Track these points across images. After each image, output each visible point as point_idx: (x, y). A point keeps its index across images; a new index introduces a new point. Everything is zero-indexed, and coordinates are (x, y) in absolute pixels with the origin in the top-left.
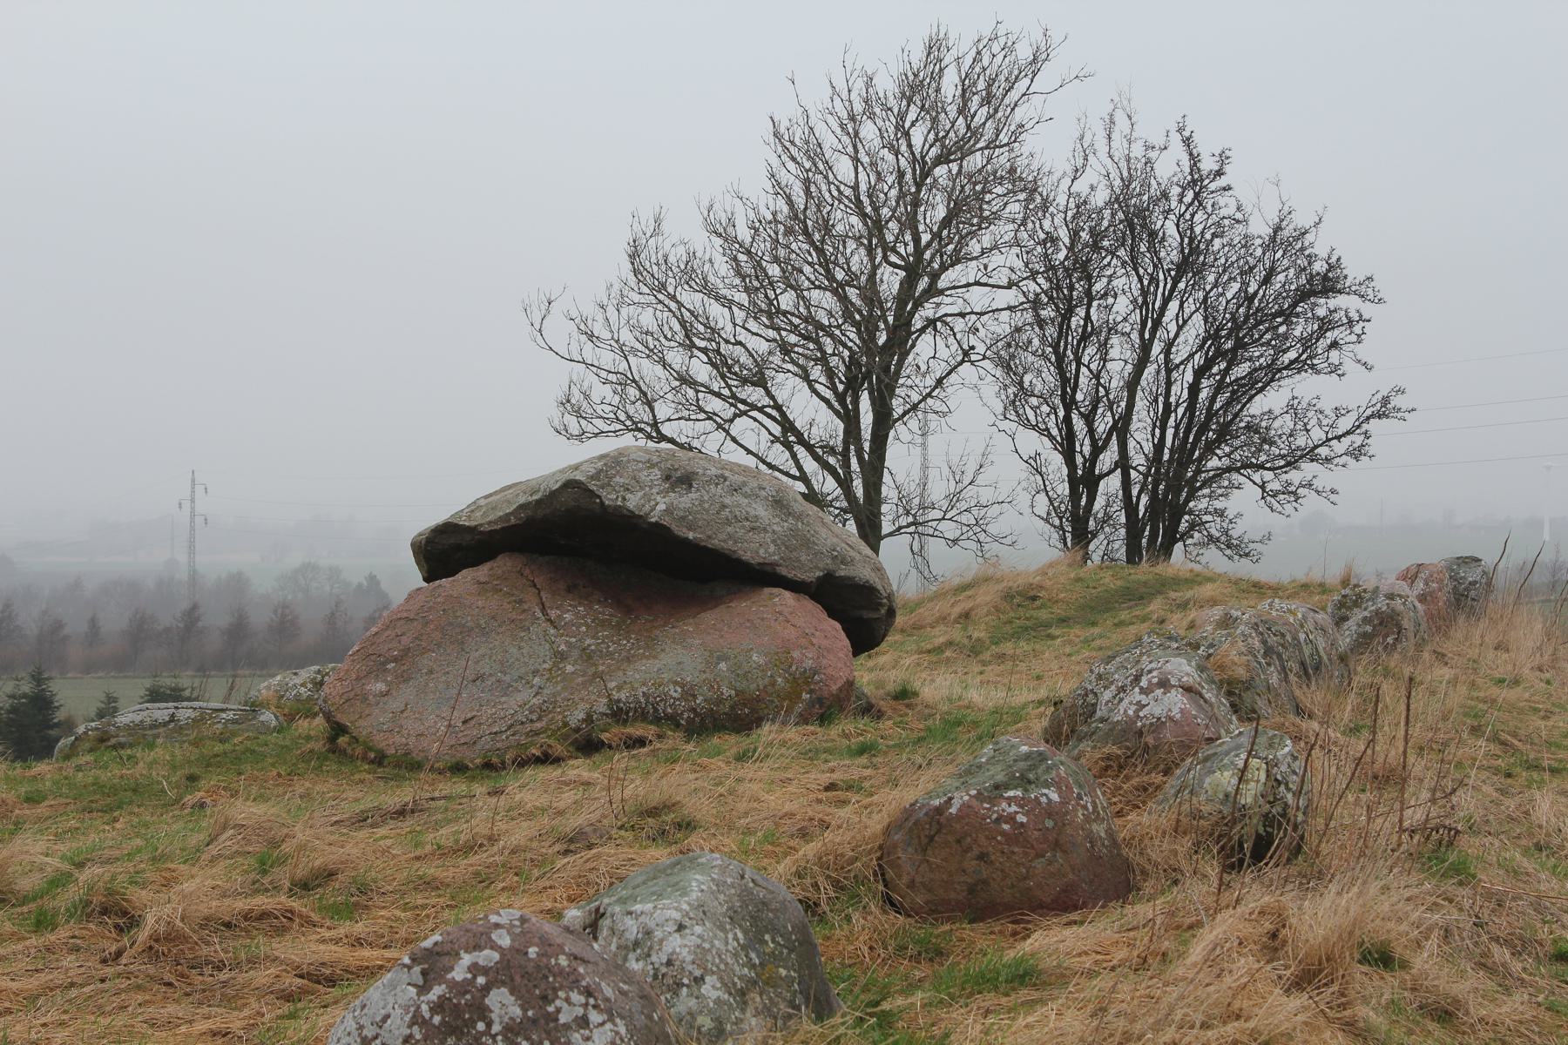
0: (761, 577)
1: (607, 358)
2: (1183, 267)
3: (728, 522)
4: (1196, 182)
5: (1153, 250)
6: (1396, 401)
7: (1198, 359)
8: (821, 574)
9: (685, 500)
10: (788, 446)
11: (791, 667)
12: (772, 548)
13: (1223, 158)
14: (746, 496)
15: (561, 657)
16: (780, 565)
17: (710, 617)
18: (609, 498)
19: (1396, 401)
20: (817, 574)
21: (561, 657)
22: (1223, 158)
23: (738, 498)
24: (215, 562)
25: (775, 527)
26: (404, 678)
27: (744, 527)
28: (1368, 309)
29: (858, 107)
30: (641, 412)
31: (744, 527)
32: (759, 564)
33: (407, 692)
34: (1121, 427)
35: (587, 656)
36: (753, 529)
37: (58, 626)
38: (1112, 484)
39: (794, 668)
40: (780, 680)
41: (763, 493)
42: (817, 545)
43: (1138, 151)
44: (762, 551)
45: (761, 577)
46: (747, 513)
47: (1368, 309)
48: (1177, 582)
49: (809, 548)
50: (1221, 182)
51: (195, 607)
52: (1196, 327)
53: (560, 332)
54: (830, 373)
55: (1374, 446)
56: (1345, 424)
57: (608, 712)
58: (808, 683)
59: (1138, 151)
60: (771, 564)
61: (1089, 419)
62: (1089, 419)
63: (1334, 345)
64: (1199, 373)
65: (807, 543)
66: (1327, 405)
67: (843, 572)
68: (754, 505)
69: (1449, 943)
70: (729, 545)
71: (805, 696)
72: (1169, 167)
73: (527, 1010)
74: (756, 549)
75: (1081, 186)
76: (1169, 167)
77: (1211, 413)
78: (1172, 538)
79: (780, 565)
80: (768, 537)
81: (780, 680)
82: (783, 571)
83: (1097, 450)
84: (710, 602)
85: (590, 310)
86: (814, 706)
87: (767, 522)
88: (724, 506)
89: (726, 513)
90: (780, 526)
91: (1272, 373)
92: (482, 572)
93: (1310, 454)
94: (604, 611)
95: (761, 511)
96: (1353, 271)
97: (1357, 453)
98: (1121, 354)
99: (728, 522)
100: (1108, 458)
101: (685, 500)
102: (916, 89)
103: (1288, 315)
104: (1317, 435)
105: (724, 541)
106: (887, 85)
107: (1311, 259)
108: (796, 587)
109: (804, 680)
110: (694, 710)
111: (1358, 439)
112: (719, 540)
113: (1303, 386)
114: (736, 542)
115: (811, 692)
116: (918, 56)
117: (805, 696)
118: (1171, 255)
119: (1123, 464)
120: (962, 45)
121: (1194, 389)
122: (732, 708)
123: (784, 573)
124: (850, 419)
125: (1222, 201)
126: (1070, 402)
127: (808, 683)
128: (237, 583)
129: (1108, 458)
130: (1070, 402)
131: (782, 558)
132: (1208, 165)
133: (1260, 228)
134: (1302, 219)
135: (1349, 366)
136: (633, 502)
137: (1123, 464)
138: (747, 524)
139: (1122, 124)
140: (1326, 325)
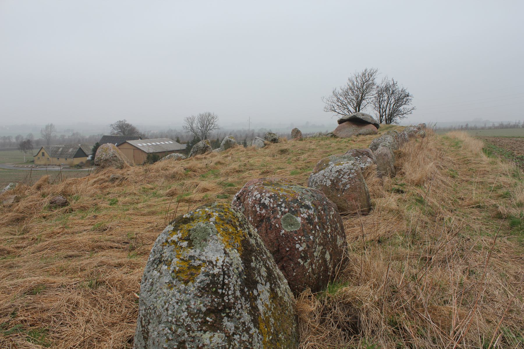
0: (369, 123)
1: (329, 103)
2: (392, 93)
4: (394, 84)
5: (389, 92)
6: (415, 108)
7: (394, 103)
9: (364, 117)
10: (348, 112)
13: (397, 82)
15: (354, 130)
17: (366, 127)
18: (357, 117)
19: (415, 108)
21: (354, 130)
22: (397, 82)
24: (252, 128)
26: (340, 131)
28: (412, 98)
29: (357, 76)
30: (333, 109)
33: (341, 132)
34: (385, 111)
35: (356, 129)
37: (237, 136)
38: (384, 117)
43: (388, 81)
45: (369, 123)
47: (412, 98)
48: (393, 126)
50: (396, 85)
51: (253, 133)
52: (393, 100)
53: (325, 100)
54: (353, 104)
55: (412, 113)
56: (409, 110)
59: (388, 81)
61: (382, 109)
62: (382, 109)
63: (408, 102)
64: (394, 105)
66: (407, 108)
69: (323, 332)
72: (391, 83)
74: (369, 121)
75: (382, 85)
76: (391, 83)
77: (395, 109)
78: (391, 122)
83: (383, 113)
84: (365, 125)
85: (328, 98)
90: (371, 119)
91: (401, 105)
92: (346, 123)
93: (405, 113)
94: (356, 126)
95: (369, 118)
96: (410, 94)
97: (411, 113)
98: (386, 103)
100: (384, 114)
101: (364, 117)
102: (364, 74)
103: (403, 99)
104: (406, 111)
106: (360, 74)
107: (406, 93)
108: (372, 124)
109: (374, 131)
111: (410, 112)
112: (366, 120)
113: (405, 106)
116: (364, 71)
118: (391, 92)
119: (385, 115)
120: (368, 71)
121: (393, 106)
124: (356, 110)
125: (396, 86)
126: (380, 108)
128: (253, 130)
129: (384, 114)
130: (380, 108)
132: (395, 83)
133: (400, 89)
134: (405, 89)
135: (410, 104)
136: (359, 117)
137: (385, 115)
139: (386, 78)
140: (407, 100)
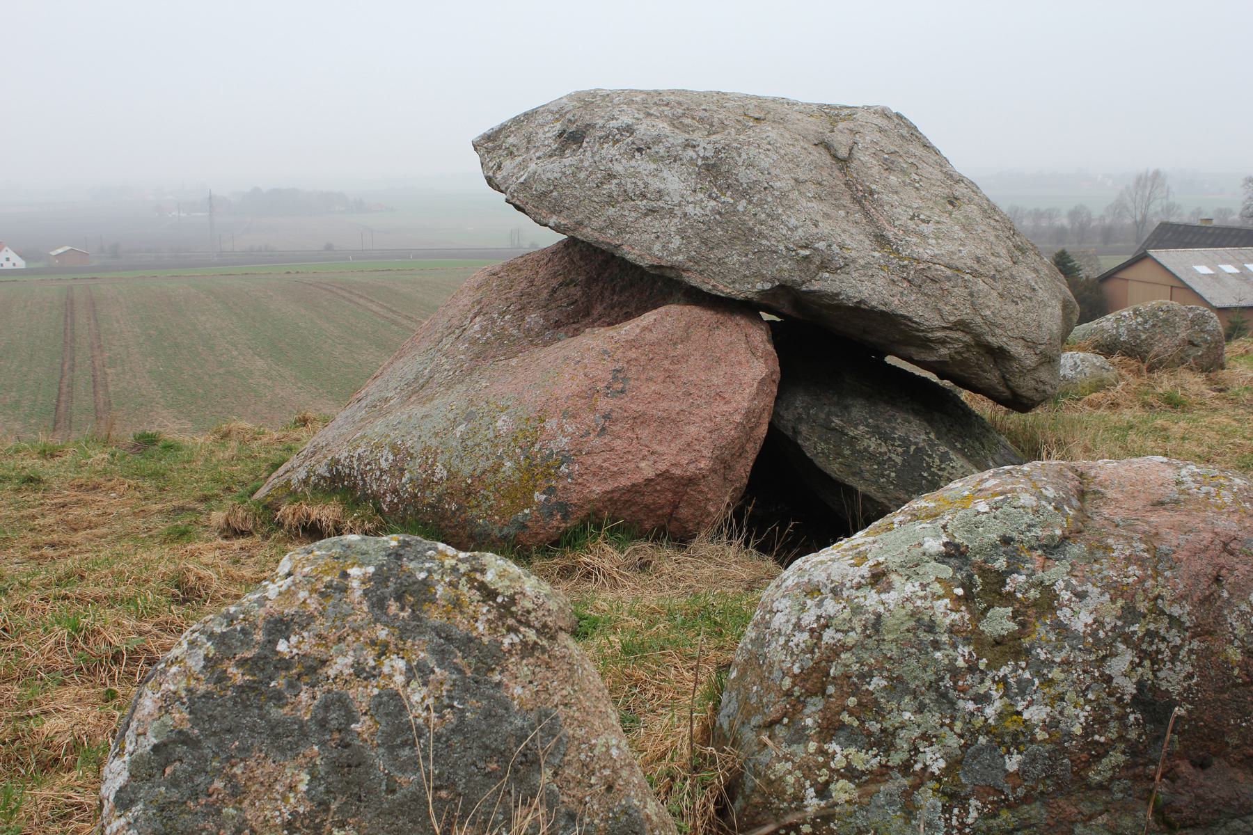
3: (611, 201)
8: (768, 286)
11: (533, 444)
12: (677, 242)
14: (657, 159)
16: (688, 270)
20: (759, 286)
23: (643, 165)
25: (690, 209)
27: (636, 208)
31: (636, 208)
32: (652, 266)
36: (652, 211)
39: (537, 447)
40: (508, 464)
41: (690, 153)
42: (765, 238)
44: (657, 246)
46: (646, 185)
49: (748, 242)
57: (327, 475)
58: (547, 476)
60: (672, 268)
65: (745, 235)
67: (823, 283)
68: (665, 174)
70: (609, 237)
71: (539, 497)
73: (796, 685)
79: (688, 270)
80: (673, 225)
81: (508, 464)
82: (694, 280)
86: (551, 515)
87: (677, 199)
88: (611, 176)
89: (612, 186)
90: (700, 207)
95: (674, 183)
99: (611, 201)
105: (601, 230)
110: (395, 491)
114: (620, 232)
115: (550, 491)
117: (539, 497)
122: (440, 498)
123: (694, 283)
127: (547, 476)
131: (690, 259)
138: (642, 204)
